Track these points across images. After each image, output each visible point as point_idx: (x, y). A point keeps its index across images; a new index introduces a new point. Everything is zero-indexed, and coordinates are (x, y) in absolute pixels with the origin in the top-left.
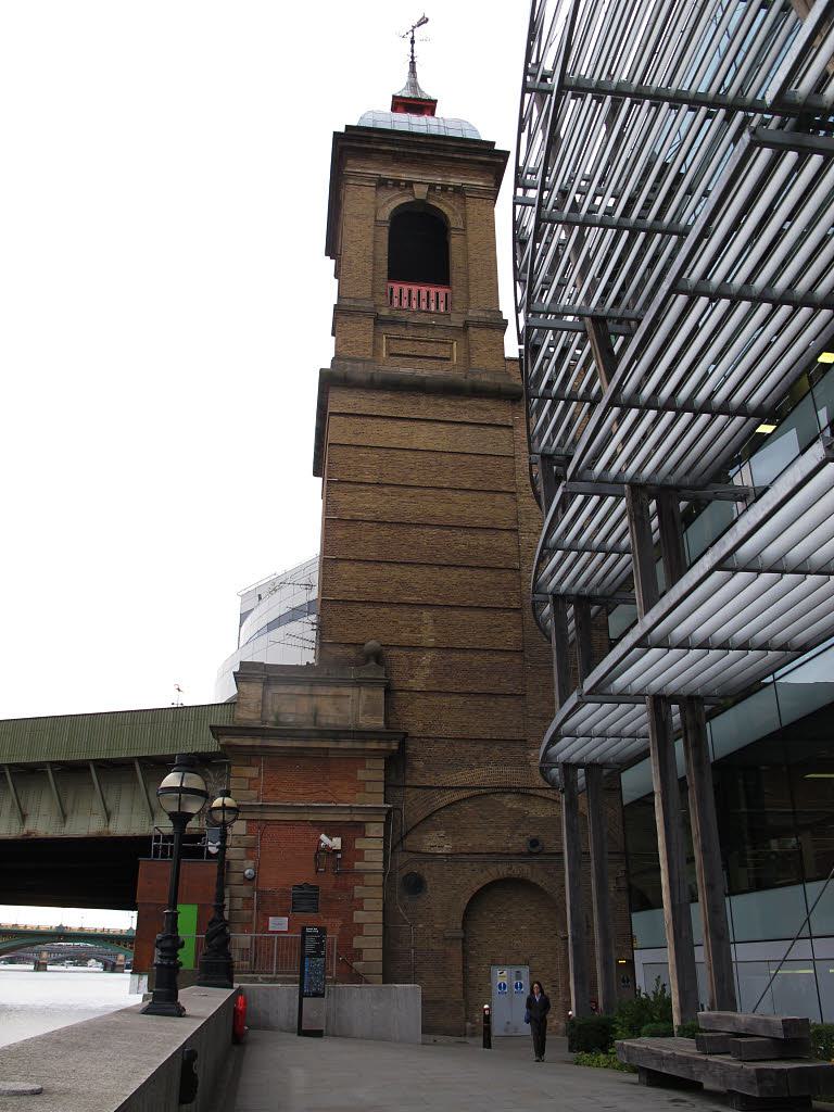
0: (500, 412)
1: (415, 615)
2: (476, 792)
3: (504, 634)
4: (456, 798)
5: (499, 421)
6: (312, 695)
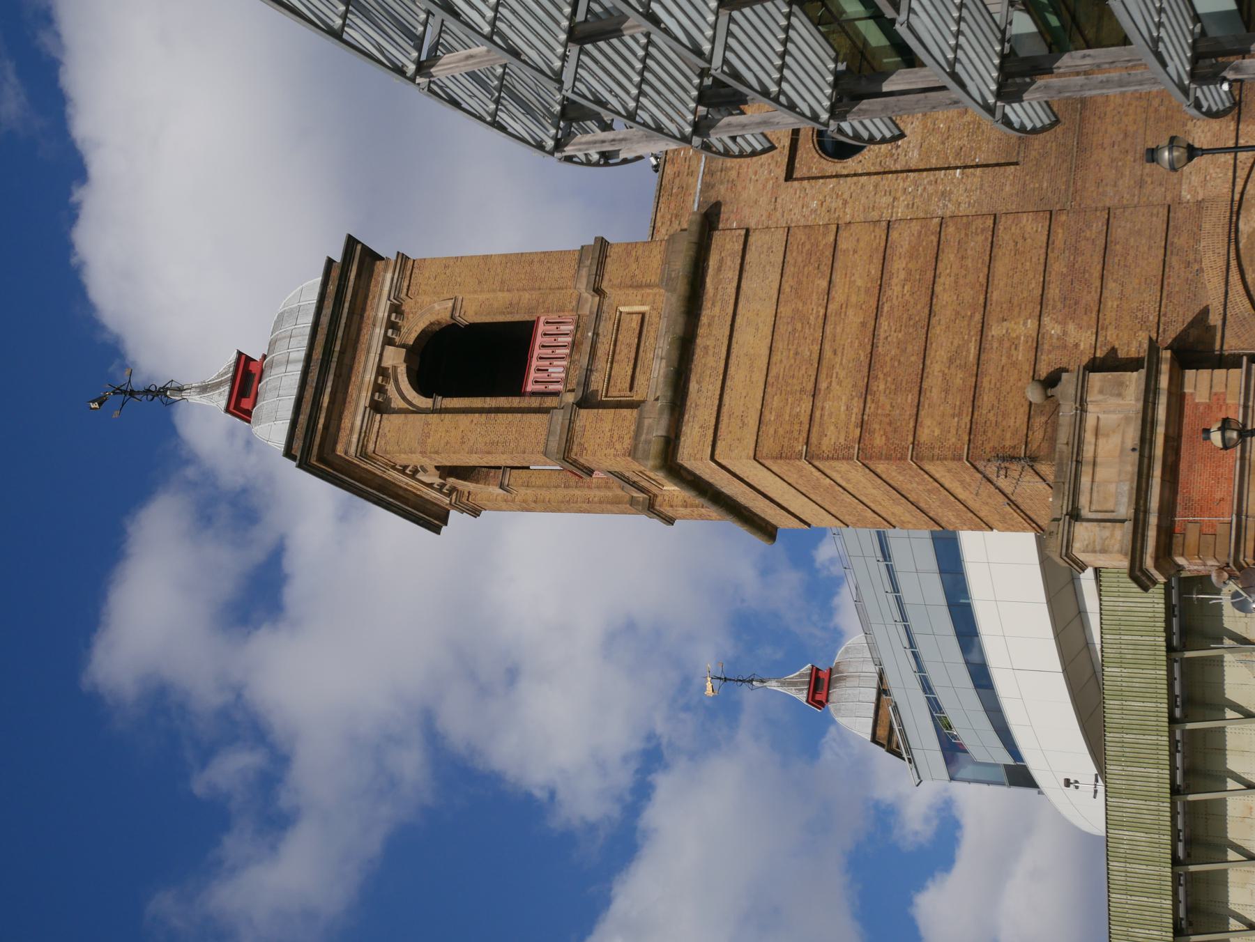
0: (724, 247)
1: (995, 345)
2: (1233, 263)
3: (1027, 236)
4: (1240, 287)
5: (738, 247)
6: (1094, 464)
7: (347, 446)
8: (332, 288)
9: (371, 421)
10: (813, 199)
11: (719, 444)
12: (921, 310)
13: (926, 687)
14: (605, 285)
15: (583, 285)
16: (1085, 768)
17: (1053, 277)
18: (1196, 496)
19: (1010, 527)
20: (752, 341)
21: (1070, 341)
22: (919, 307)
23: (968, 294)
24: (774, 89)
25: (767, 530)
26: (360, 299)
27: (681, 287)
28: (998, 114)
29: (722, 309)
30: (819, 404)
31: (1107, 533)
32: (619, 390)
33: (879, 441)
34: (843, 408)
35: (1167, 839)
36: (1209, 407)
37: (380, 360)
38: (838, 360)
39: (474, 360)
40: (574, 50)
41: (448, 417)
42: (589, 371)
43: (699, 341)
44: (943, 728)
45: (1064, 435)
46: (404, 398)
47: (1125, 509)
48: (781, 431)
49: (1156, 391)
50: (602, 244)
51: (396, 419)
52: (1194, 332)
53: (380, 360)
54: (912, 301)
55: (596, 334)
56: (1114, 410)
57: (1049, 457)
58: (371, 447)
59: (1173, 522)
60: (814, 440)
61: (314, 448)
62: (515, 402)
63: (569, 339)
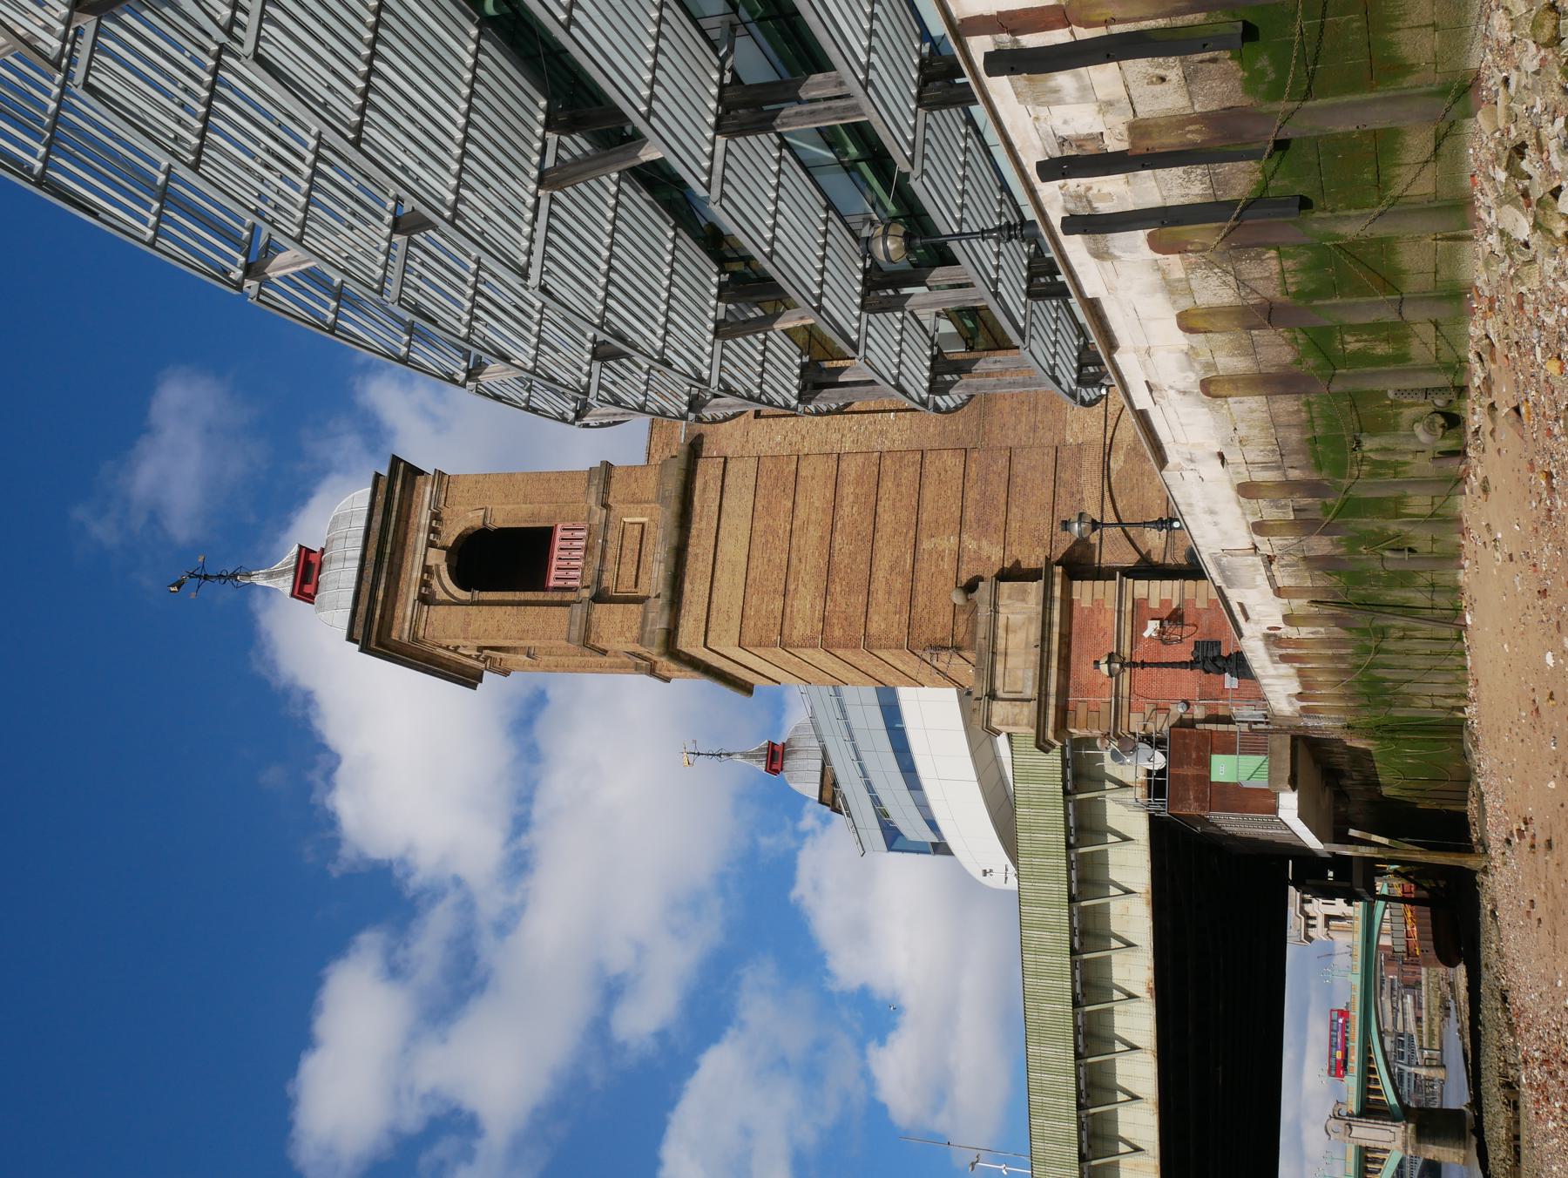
0: (707, 472)
2: (1107, 494)
7: (401, 631)
8: (380, 498)
9: (420, 612)
11: (710, 634)
12: (866, 528)
13: (869, 787)
14: (610, 501)
15: (592, 501)
16: (999, 858)
17: (969, 503)
18: (1084, 682)
19: (935, 684)
21: (984, 554)
23: (903, 515)
24: (757, 391)
25: (747, 688)
26: (405, 506)
27: (674, 506)
28: (931, 405)
30: (789, 602)
31: (1017, 710)
32: (626, 587)
33: (838, 633)
35: (1067, 936)
36: (1092, 610)
39: (503, 560)
40: (596, 365)
41: (485, 609)
42: (601, 571)
43: (690, 549)
44: (883, 817)
45: (982, 631)
46: (447, 592)
47: (1030, 691)
49: (1052, 598)
50: (608, 467)
51: (441, 611)
52: (1079, 549)
55: (605, 541)
56: (1019, 610)
57: (971, 648)
58: (421, 633)
59: (1067, 702)
60: (786, 631)
61: (373, 633)
62: (540, 596)
63: (583, 543)
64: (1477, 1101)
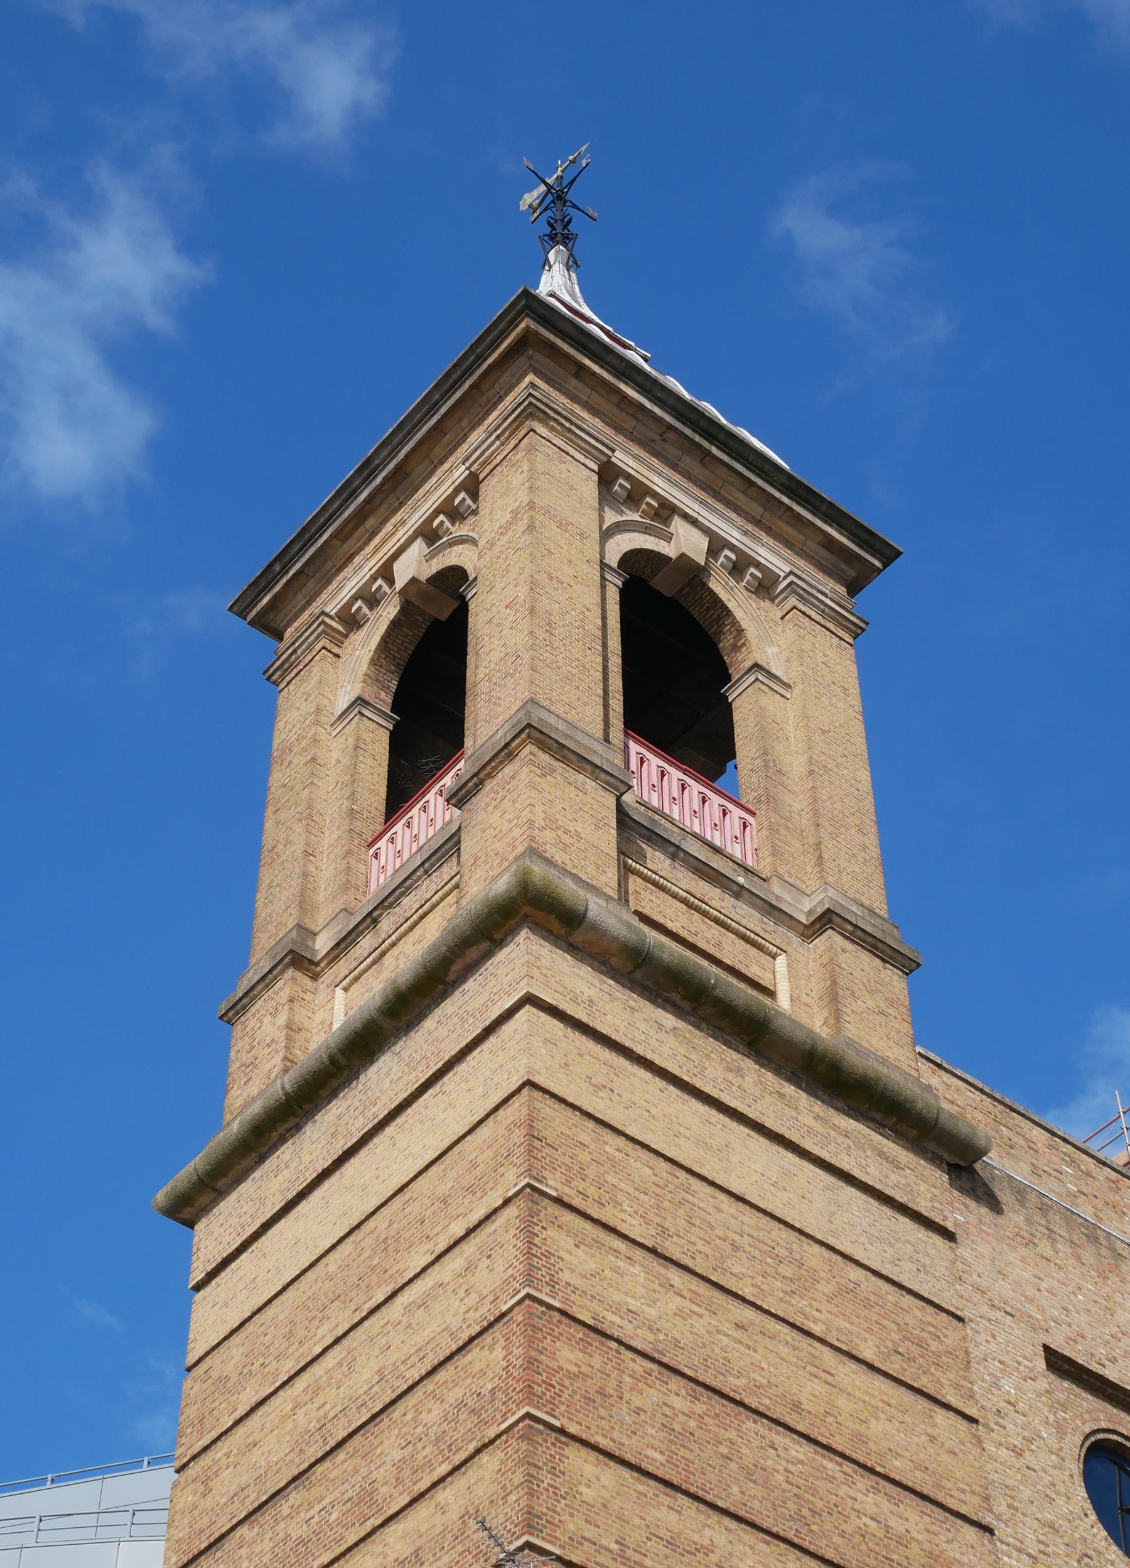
10: (1018, 1389)
14: (830, 938)
20: (752, 1165)
22: (837, 1539)
29: (810, 1131)
34: (633, 1304)
37: (685, 517)
38: (727, 1327)
48: (584, 1157)
53: (685, 517)
54: (849, 1528)
64: (706, 531)
